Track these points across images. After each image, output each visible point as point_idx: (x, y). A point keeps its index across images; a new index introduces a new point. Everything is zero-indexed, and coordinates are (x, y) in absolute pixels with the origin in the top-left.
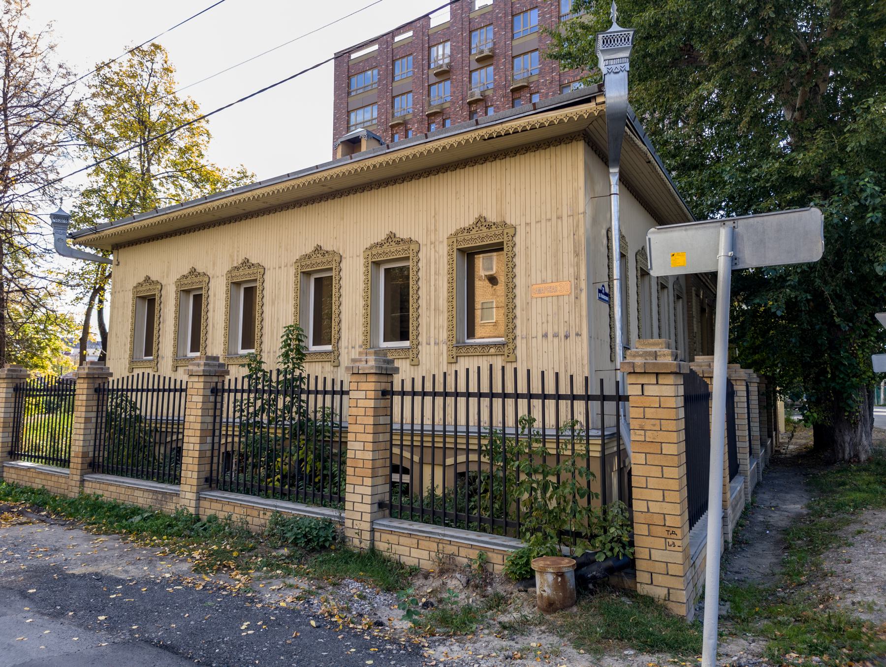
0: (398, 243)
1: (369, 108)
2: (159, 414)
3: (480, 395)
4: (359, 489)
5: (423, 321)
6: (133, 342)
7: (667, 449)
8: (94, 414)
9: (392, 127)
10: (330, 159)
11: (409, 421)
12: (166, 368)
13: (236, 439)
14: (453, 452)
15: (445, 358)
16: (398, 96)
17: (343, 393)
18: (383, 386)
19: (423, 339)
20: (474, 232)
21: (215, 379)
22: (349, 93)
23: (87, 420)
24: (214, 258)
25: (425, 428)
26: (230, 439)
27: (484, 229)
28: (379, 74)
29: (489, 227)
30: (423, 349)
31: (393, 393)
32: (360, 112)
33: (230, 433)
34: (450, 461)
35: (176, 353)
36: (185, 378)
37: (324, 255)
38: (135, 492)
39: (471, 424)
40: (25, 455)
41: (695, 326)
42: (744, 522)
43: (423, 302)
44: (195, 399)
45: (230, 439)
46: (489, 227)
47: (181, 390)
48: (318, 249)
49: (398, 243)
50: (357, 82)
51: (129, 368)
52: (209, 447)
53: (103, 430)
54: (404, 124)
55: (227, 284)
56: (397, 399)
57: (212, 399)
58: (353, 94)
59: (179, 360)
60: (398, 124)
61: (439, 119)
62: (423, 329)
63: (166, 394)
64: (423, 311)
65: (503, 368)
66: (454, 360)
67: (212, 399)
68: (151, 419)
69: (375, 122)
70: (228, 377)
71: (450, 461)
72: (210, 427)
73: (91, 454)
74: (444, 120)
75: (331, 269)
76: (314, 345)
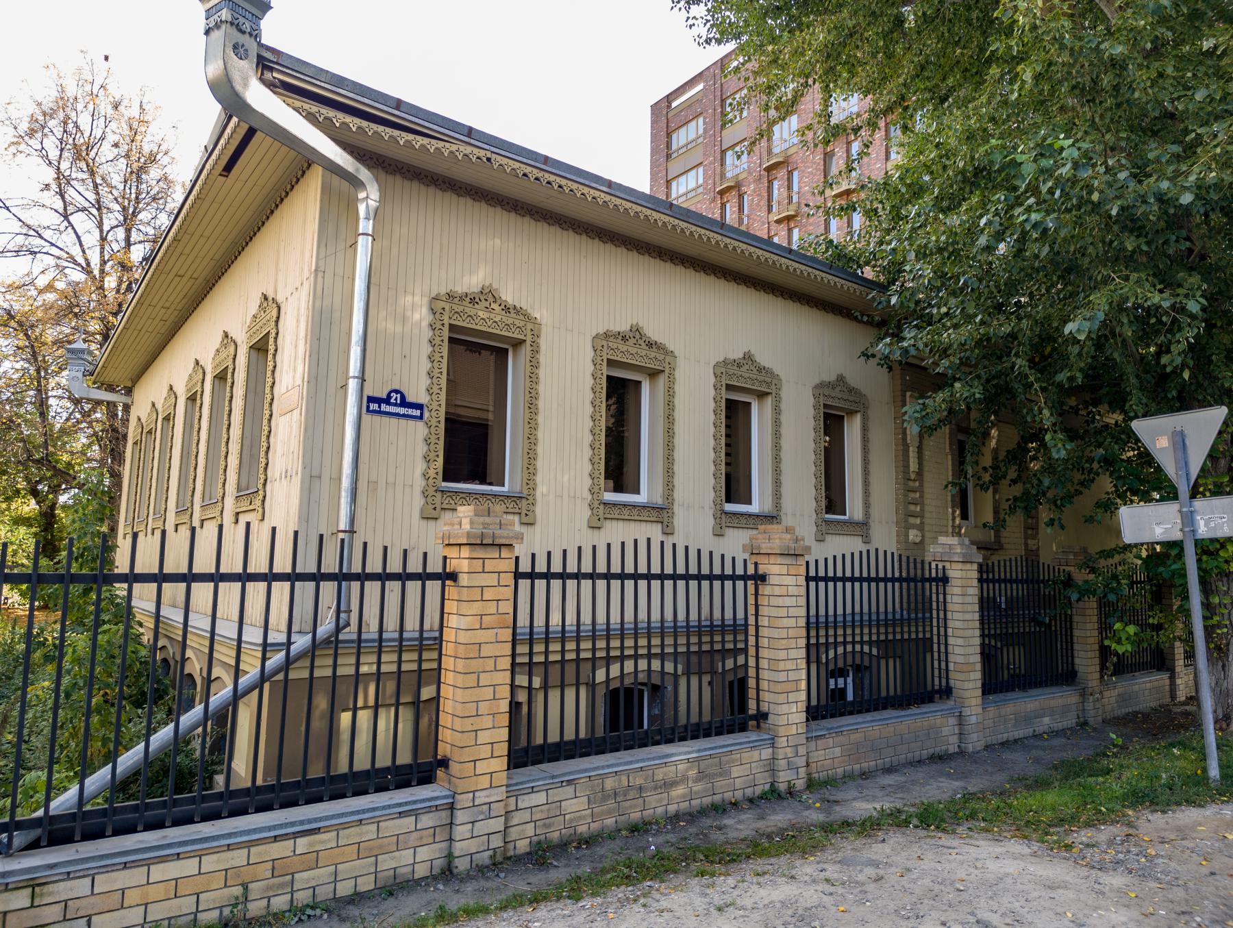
1: (693, 172)
7: (960, 641)
9: (722, 193)
11: (374, 627)
13: (849, 648)
14: (604, 662)
16: (728, 149)
22: (668, 156)
25: (640, 626)
26: (840, 650)
28: (705, 123)
32: (682, 179)
33: (849, 639)
34: (600, 676)
39: (568, 622)
41: (911, 460)
45: (840, 650)
48: (748, 357)
50: (681, 138)
53: (935, 640)
54: (737, 186)
58: (674, 156)
60: (729, 189)
61: (782, 173)
63: (873, 575)
65: (662, 543)
68: (853, 613)
69: (701, 190)
71: (600, 676)
74: (790, 173)
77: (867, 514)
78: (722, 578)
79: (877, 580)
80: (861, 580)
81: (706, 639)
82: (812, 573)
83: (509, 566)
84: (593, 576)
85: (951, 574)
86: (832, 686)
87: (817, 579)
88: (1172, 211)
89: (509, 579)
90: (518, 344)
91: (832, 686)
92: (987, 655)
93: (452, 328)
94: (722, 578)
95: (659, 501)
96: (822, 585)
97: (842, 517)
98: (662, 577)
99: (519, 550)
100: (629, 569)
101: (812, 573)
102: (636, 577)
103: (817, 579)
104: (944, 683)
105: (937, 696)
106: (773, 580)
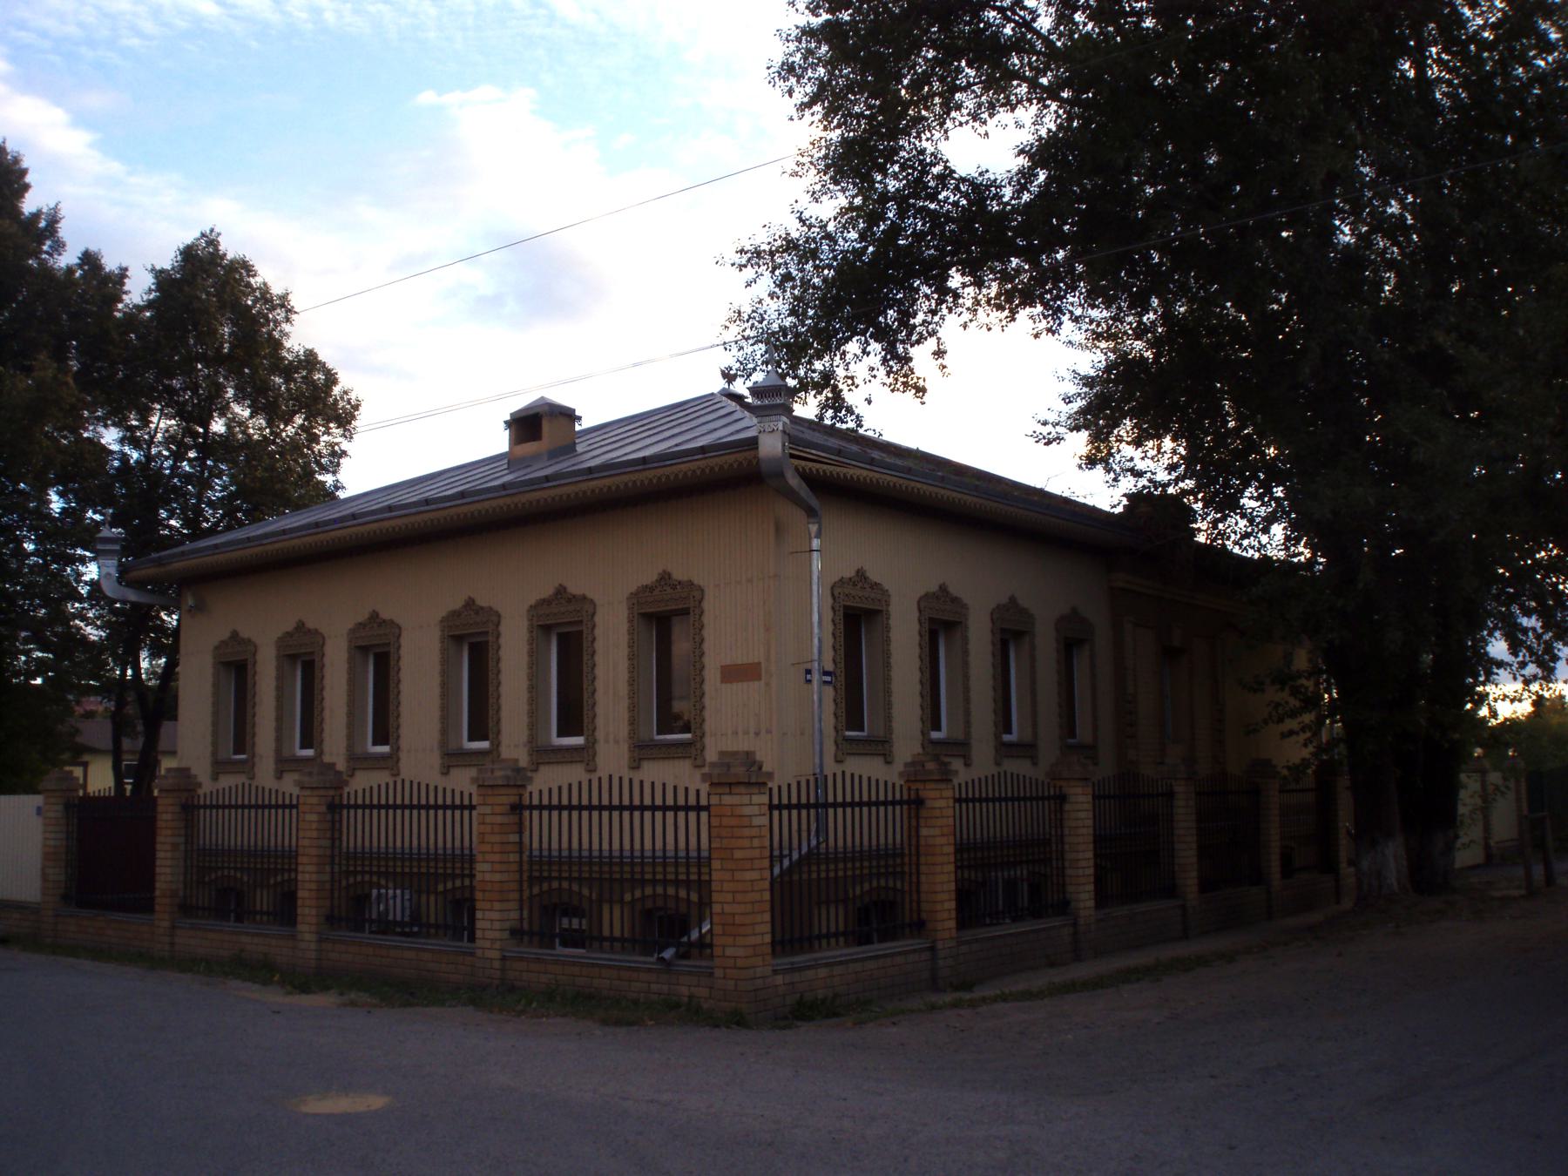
0: (569, 601)
2: (545, 839)
3: (642, 808)
4: (489, 915)
5: (599, 710)
6: (215, 734)
8: (182, 840)
10: (506, 449)
12: (613, 757)
15: (625, 761)
17: (472, 807)
18: (514, 799)
19: (600, 734)
20: (656, 592)
21: (331, 793)
23: (175, 846)
24: (334, 611)
27: (669, 590)
29: (674, 587)
30: (601, 748)
31: (342, 806)
35: (278, 751)
36: (296, 791)
37: (477, 613)
38: (254, 941)
40: (819, 937)
42: (263, 900)
43: (599, 684)
44: (309, 817)
46: (674, 587)
47: (291, 806)
49: (569, 601)
51: (443, 765)
52: (327, 877)
55: (278, 657)
56: (527, 813)
57: (329, 817)
59: (284, 764)
62: (600, 721)
64: (599, 696)
66: (635, 765)
67: (329, 817)
70: (346, 790)
72: (328, 852)
73: (181, 893)
75: (486, 633)
76: (560, 735)
77: (1035, 734)
78: (445, 807)
79: (877, 804)
80: (1013, 799)
81: (866, 864)
82: (776, 801)
83: (765, 799)
84: (395, 807)
85: (923, 794)
86: (584, 922)
87: (780, 807)
88: (807, 408)
89: (765, 809)
90: (878, 612)
91: (584, 922)
92: (1099, 880)
93: (845, 607)
94: (445, 807)
95: (960, 736)
96: (595, 814)
97: (370, 740)
98: (372, 807)
99: (773, 785)
100: (605, 802)
101: (776, 801)
102: (570, 808)
103: (780, 807)
104: (915, 916)
105: (907, 931)
106: (929, 803)
